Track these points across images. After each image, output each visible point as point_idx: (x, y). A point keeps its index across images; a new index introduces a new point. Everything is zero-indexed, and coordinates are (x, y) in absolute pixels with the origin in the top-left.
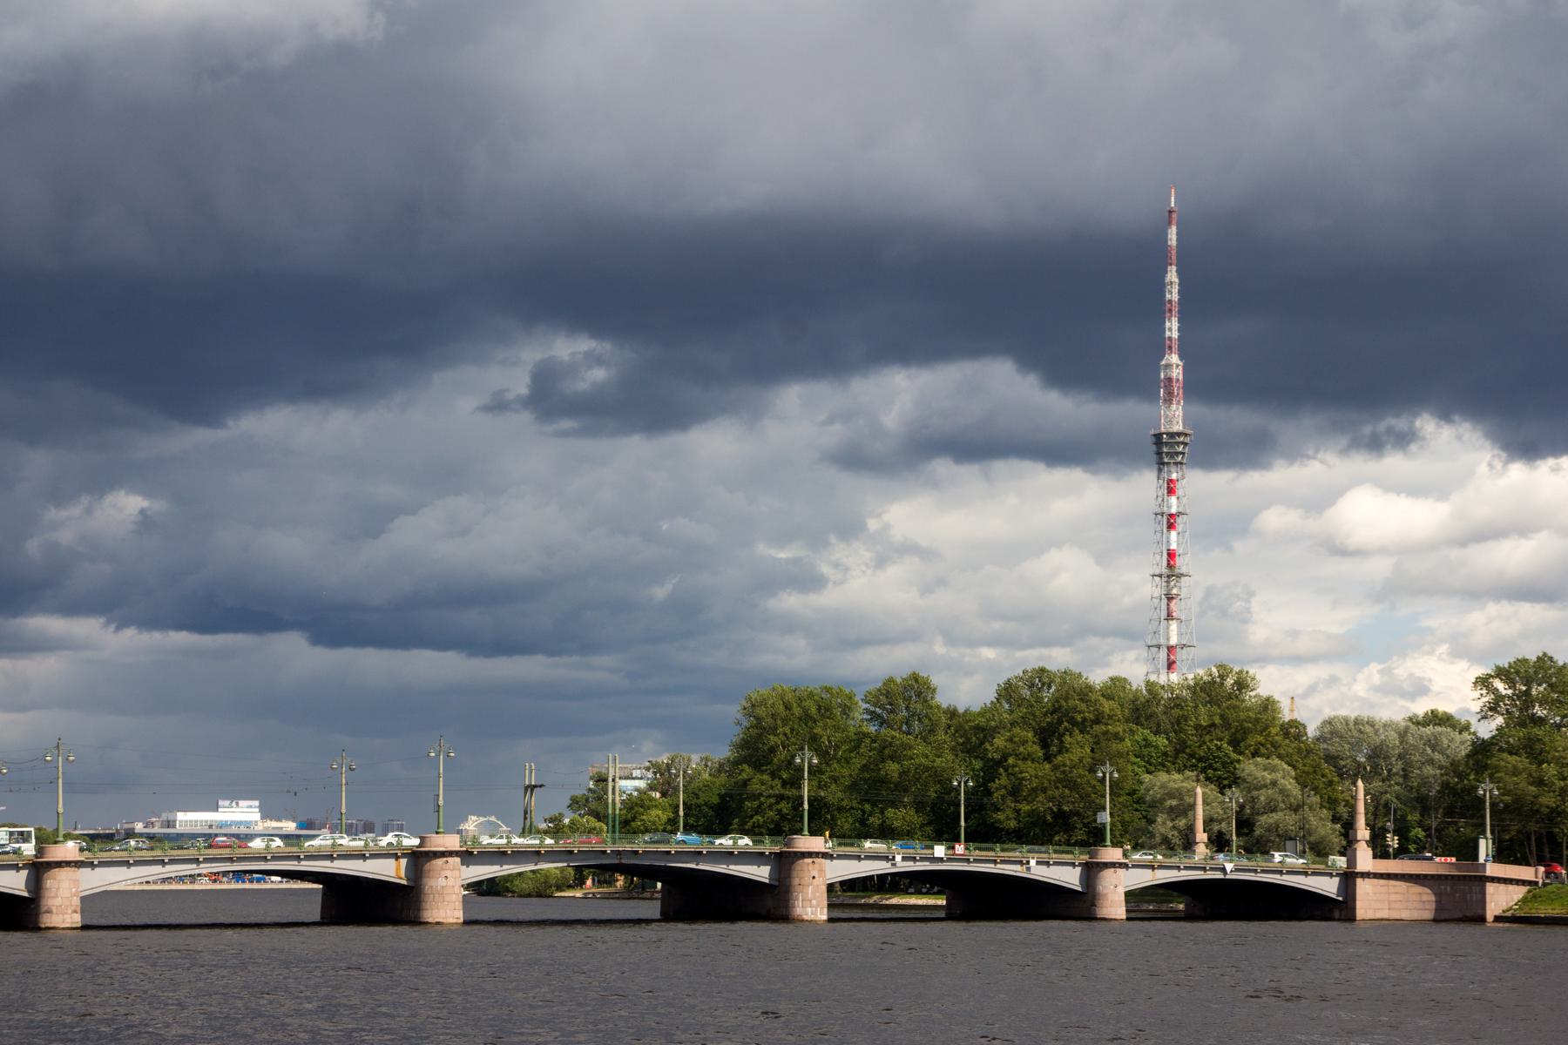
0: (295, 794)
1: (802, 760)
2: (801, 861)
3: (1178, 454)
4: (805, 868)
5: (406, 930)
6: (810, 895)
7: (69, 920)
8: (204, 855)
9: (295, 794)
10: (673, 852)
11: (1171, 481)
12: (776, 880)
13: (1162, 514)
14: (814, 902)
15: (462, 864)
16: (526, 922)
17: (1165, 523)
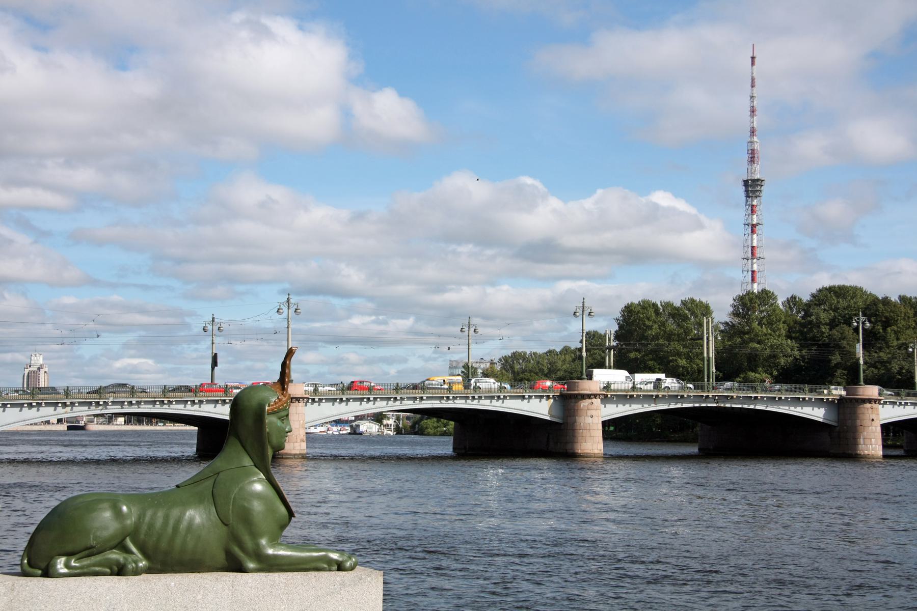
1: (858, 323)
2: (862, 406)
3: (757, 191)
4: (866, 411)
5: (842, 469)
7: (298, 448)
11: (753, 205)
12: (835, 422)
13: (748, 225)
15: (601, 404)
16: (35, 434)
17: (750, 229)
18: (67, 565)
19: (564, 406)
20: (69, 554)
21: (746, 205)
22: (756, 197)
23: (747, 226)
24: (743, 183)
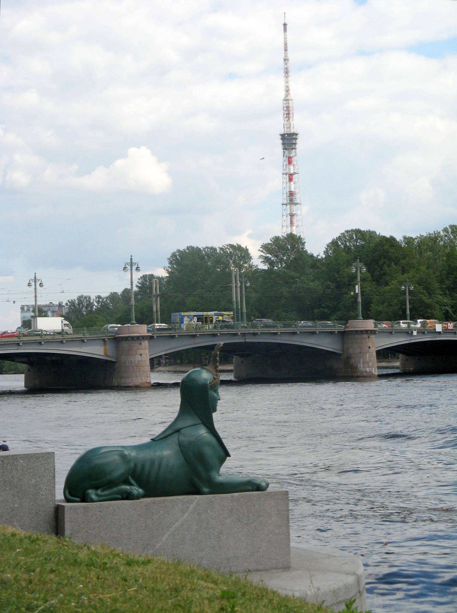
0: (14, 302)
6: (368, 359)
9: (14, 302)
12: (341, 350)
13: (286, 174)
14: (370, 364)
16: (144, 388)
18: (97, 495)
21: (283, 157)
22: (293, 149)
23: (285, 175)
24: (280, 137)
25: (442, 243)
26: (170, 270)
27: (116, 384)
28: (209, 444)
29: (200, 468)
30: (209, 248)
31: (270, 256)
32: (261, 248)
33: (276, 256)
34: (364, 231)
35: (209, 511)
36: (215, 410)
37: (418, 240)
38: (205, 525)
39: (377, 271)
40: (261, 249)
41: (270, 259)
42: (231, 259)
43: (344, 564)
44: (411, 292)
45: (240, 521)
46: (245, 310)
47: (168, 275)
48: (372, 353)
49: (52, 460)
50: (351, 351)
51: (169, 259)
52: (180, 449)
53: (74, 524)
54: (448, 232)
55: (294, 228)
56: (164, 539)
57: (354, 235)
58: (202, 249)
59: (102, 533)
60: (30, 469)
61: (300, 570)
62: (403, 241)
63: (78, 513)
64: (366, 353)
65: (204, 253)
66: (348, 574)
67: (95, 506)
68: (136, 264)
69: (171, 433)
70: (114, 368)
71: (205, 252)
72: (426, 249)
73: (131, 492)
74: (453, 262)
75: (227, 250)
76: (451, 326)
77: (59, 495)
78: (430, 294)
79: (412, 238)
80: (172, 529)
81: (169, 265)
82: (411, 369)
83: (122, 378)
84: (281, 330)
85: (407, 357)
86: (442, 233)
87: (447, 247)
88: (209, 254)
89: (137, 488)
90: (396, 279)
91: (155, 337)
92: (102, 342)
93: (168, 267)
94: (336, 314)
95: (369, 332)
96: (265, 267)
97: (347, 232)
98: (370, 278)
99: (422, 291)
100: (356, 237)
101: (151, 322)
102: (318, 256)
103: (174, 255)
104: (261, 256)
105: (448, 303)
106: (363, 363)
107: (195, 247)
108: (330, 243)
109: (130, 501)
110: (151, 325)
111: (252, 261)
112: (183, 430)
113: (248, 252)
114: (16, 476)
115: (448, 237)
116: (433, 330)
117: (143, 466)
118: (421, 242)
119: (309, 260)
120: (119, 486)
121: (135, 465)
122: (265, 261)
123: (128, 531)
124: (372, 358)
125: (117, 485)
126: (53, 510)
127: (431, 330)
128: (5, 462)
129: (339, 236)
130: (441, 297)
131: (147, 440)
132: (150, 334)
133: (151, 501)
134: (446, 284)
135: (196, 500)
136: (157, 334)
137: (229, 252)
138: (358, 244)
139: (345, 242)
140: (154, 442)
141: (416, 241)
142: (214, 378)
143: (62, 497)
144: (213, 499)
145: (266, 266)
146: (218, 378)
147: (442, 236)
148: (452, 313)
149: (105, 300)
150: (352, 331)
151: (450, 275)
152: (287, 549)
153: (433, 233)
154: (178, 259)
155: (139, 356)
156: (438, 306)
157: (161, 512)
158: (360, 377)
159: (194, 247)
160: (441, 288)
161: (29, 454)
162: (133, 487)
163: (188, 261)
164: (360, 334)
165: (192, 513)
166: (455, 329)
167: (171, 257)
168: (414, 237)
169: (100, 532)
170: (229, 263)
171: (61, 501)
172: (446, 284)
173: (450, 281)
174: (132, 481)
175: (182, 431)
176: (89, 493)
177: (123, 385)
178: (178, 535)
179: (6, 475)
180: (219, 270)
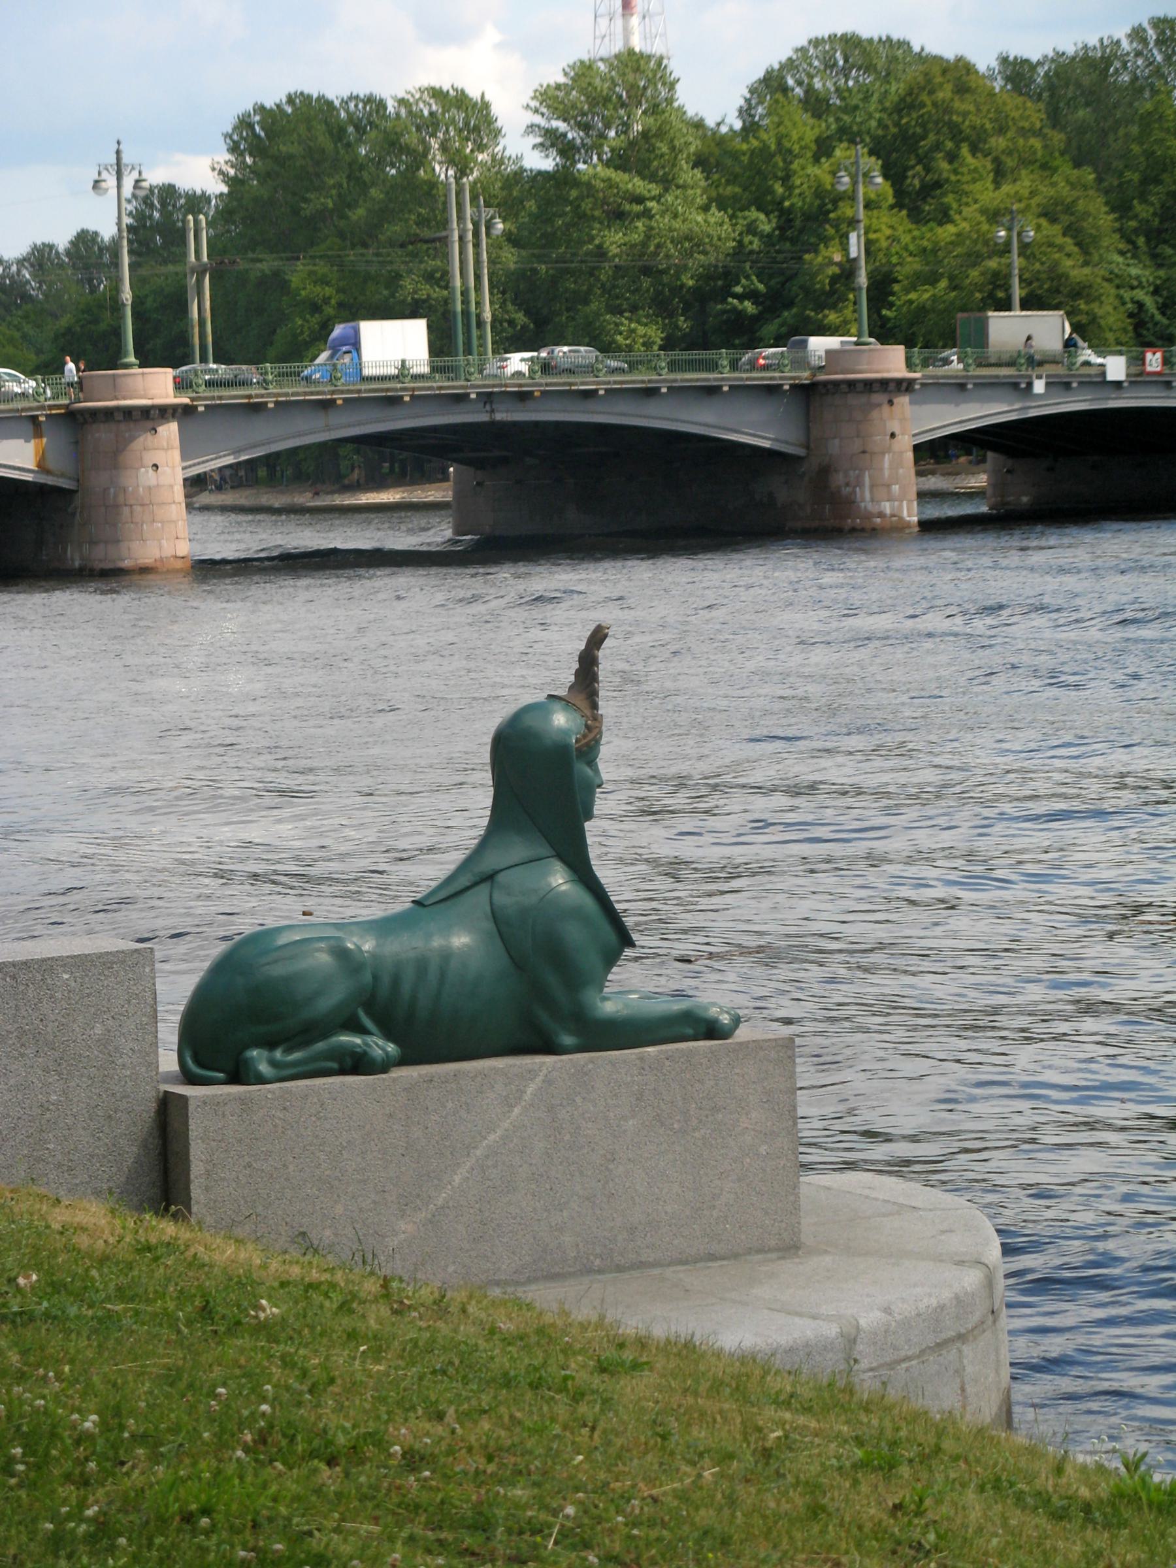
6: (887, 473)
8: (205, 399)
10: (787, 387)
12: (800, 446)
14: (896, 488)
18: (273, 1063)
19: (77, 443)
20: (271, 1045)
25: (1126, 78)
26: (232, 172)
27: (77, 564)
28: (576, 913)
29: (552, 981)
30: (363, 101)
31: (561, 126)
32: (533, 99)
33: (586, 127)
34: (870, 41)
35: (579, 1100)
36: (589, 816)
37: (1046, 68)
38: (567, 1137)
39: (914, 177)
40: (534, 104)
41: (565, 135)
42: (433, 135)
43: (943, 1232)
44: (1024, 247)
45: (662, 1124)
46: (487, 315)
47: (225, 189)
48: (901, 453)
49: (147, 970)
50: (834, 447)
51: (227, 136)
52: (495, 929)
53: (214, 1144)
54: (1144, 41)
55: (635, 21)
56: (457, 1179)
57: (838, 54)
58: (337, 103)
59: (291, 1168)
60: (88, 995)
61: (826, 1252)
62: (1000, 72)
63: (224, 1115)
64: (883, 453)
65: (343, 114)
66: (960, 1263)
67: (269, 1096)
68: (133, 168)
69: (468, 884)
70: (70, 510)
71: (347, 111)
72: (1074, 98)
73: (365, 1053)
74: (1163, 140)
75: (421, 105)
76: (1154, 361)
77: (169, 1061)
78: (1086, 252)
79: (1027, 61)
80: (478, 1153)
81: (228, 157)
82: (1025, 499)
83: (93, 543)
84: (609, 383)
85: (1010, 463)
86: (1126, 45)
87: (1141, 90)
88: (360, 120)
89: (380, 1042)
90: (976, 201)
91: (201, 409)
92: (29, 428)
93: (226, 163)
94: (779, 316)
95: (892, 386)
96: (542, 162)
97: (816, 42)
98: (891, 200)
99: (1060, 240)
100: (846, 60)
101: (185, 359)
102: (719, 124)
103: (244, 123)
104: (532, 126)
105: (1144, 280)
106: (872, 486)
107: (315, 96)
108: (760, 81)
109: (363, 1078)
110: (184, 368)
111: (503, 142)
112: (502, 874)
113: (488, 114)
114: (53, 1018)
115: (1147, 59)
116: (1096, 375)
117: (396, 981)
118: (1057, 74)
119: (691, 139)
120: (332, 1035)
121: (375, 977)
122: (548, 143)
123: (359, 1159)
124: (901, 471)
125: (324, 1036)
126: (153, 1106)
127: (1089, 376)
128: (22, 977)
129: (790, 59)
130: (1120, 259)
131: (402, 905)
132: (186, 401)
133: (420, 1075)
134: (1136, 216)
135: (545, 1071)
136: (205, 399)
137: (426, 113)
138: (851, 83)
139: (811, 77)
140: (420, 909)
141: (1041, 71)
142: (587, 727)
143: (175, 1067)
144: (590, 1066)
145: (551, 159)
146: (597, 724)
147: (1128, 54)
148: (1156, 312)
149: (14, 268)
150: (836, 384)
151: (1151, 187)
152: (792, 1198)
153: (1098, 45)
154: (258, 137)
155: (150, 470)
156: (1113, 291)
157: (450, 1105)
158: (863, 530)
159: (309, 97)
160: (1120, 230)
161: (86, 956)
162: (370, 1039)
163: (293, 143)
164: (862, 392)
165: (532, 1105)
166: (1167, 371)
167: (234, 129)
168: (1034, 59)
169: (284, 1165)
170: (427, 149)
171: (169, 1078)
172: (1136, 216)
173: (1152, 204)
174: (368, 1023)
175: (500, 878)
176: (252, 1058)
177: (99, 566)
178: (495, 1166)
179: (25, 1014)
180: (393, 171)
